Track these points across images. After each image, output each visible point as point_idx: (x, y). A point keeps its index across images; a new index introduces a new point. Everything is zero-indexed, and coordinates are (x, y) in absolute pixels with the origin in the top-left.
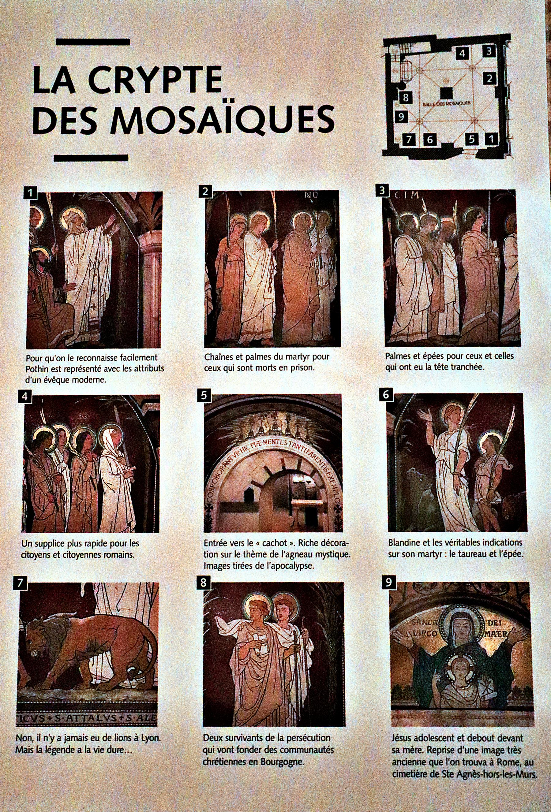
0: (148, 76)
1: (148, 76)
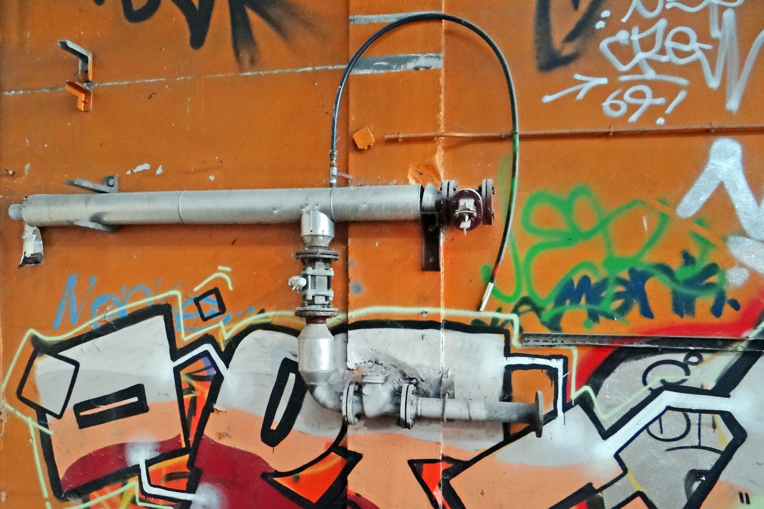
0: (157, 174)
1: (157, 174)
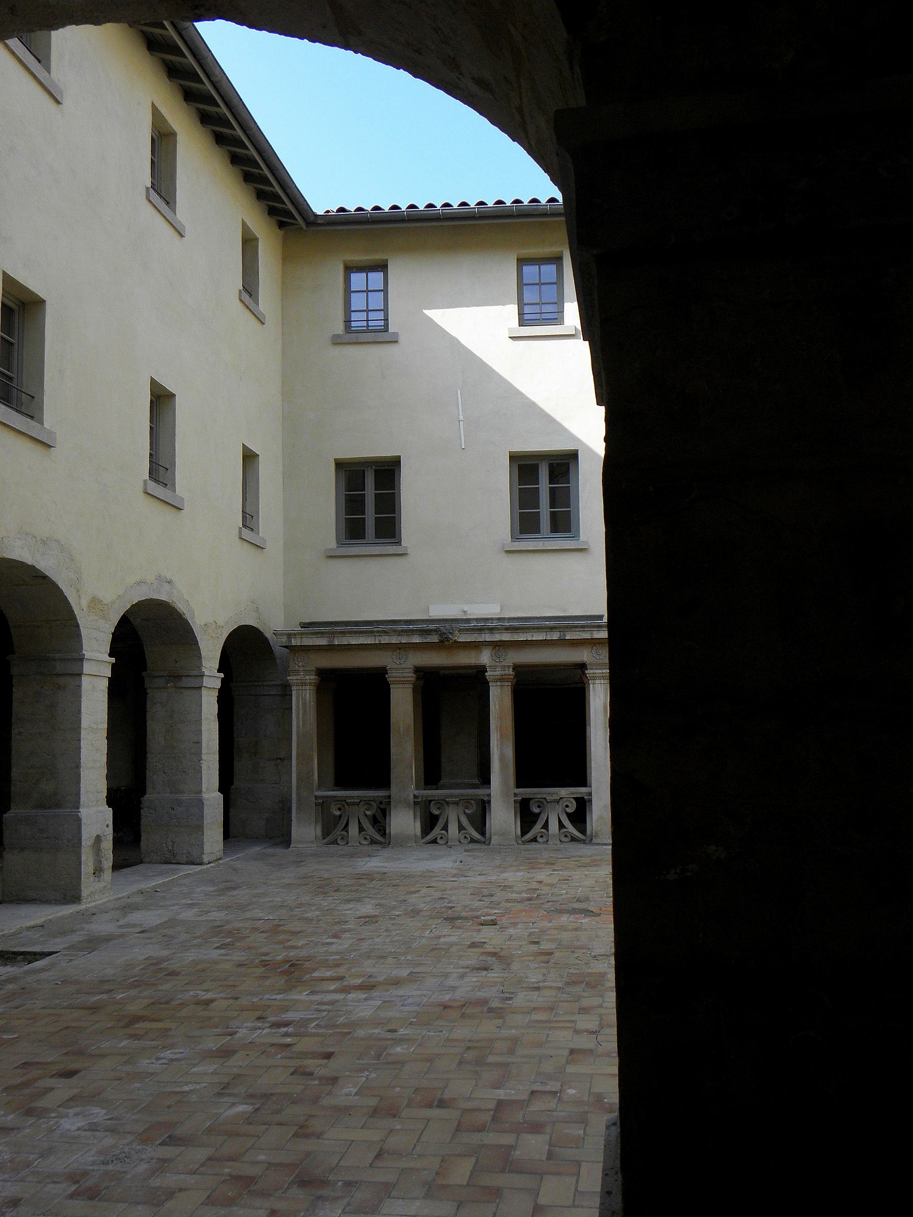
1: (424, 311)
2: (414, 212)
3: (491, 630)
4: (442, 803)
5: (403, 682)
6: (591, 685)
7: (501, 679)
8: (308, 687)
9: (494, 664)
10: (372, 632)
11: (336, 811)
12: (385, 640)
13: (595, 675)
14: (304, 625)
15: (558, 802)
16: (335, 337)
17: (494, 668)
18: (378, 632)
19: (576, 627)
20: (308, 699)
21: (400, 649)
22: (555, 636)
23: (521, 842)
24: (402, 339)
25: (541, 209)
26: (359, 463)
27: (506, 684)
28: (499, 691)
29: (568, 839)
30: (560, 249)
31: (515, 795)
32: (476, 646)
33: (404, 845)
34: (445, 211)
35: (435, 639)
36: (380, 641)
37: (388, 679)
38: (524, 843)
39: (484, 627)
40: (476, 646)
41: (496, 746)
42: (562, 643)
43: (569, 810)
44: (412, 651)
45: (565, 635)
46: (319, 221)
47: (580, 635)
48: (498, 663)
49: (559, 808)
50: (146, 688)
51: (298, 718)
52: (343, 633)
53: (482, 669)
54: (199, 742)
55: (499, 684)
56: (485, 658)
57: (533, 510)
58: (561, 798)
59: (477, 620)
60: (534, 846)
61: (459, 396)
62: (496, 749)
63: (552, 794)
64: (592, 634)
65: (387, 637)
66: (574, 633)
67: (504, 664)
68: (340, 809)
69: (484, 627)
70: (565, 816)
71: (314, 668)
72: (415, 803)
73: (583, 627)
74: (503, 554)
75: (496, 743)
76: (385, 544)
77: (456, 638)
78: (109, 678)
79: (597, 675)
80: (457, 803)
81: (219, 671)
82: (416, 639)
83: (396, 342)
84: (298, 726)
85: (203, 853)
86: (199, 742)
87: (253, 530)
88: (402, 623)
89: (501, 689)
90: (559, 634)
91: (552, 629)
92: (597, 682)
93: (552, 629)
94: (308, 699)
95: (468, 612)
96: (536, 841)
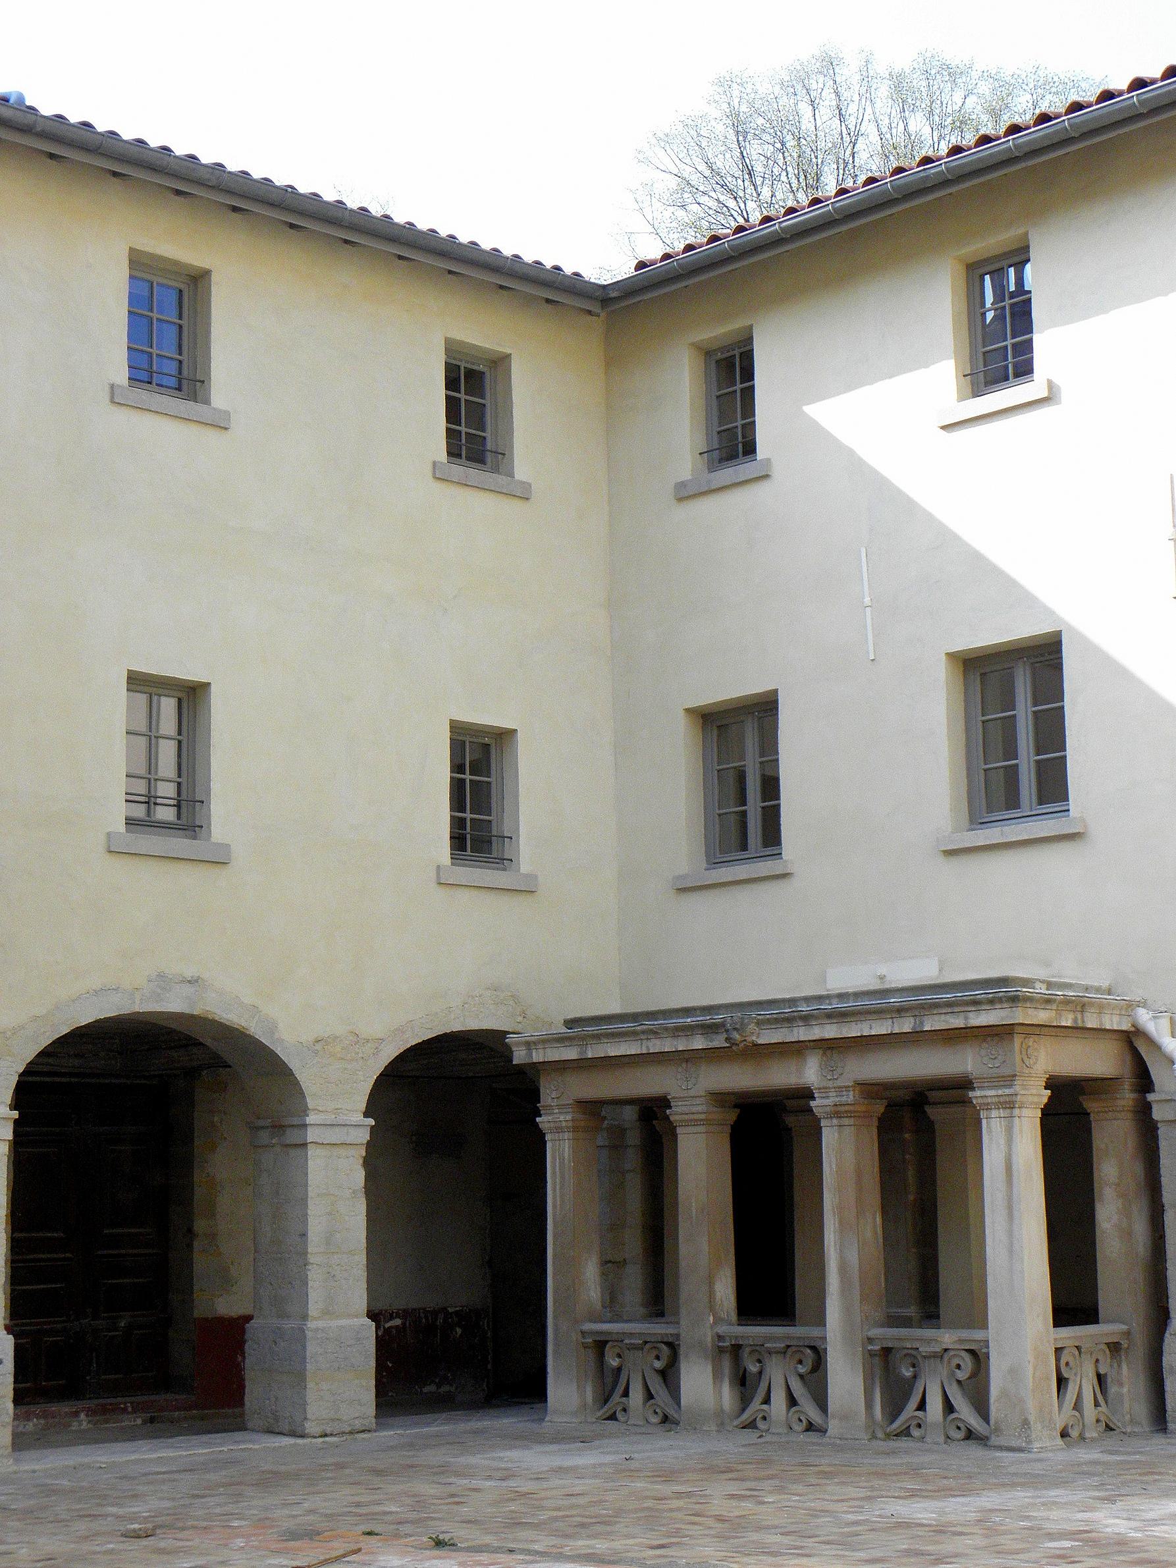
0: (806, 409)
1: (806, 409)
2: (691, 258)
3: (806, 1019)
4: (761, 1353)
5: (696, 1123)
6: (984, 1122)
7: (837, 1113)
8: (566, 1135)
9: (825, 1084)
10: (634, 1033)
11: (907, 1370)
12: (655, 1046)
13: (985, 1101)
14: (570, 1023)
15: (942, 1357)
16: (681, 485)
17: (824, 1089)
18: (643, 1032)
19: (936, 1006)
20: (566, 1155)
21: (687, 1062)
22: (906, 1025)
23: (880, 1435)
24: (777, 471)
25: (933, 174)
26: (739, 708)
27: (846, 1121)
28: (836, 1134)
29: (960, 1435)
30: (1021, 231)
31: (870, 1340)
32: (797, 1050)
33: (698, 1427)
34: (784, 224)
35: (719, 1041)
36: (649, 1049)
37: (672, 1118)
38: (888, 1436)
39: (793, 1014)
40: (797, 1050)
41: (832, 1243)
42: (916, 1038)
43: (962, 1375)
44: (703, 1068)
45: (922, 1023)
46: (614, 294)
47: (947, 1022)
48: (831, 1082)
49: (943, 1370)
50: (544, 1134)
51: (554, 1190)
52: (597, 1037)
53: (806, 1094)
54: (304, 1235)
55: (835, 1121)
56: (811, 1073)
57: (1048, 756)
58: (946, 1350)
59: (842, 996)
60: (903, 1443)
61: (864, 559)
62: (832, 1249)
63: (929, 1341)
64: (966, 1018)
65: (658, 1042)
66: (936, 1018)
67: (839, 1083)
68: (619, 1356)
69: (793, 1014)
70: (955, 1386)
71: (571, 1102)
72: (721, 1350)
73: (949, 1004)
74: (941, 859)
75: (832, 1236)
76: (764, 858)
77: (754, 1038)
78: (9, 1140)
79: (989, 1100)
80: (783, 1352)
81: (366, 1114)
82: (699, 1043)
83: (767, 476)
84: (554, 1206)
85: (306, 1418)
86: (304, 1235)
87: (511, 860)
88: (698, 1012)
89: (839, 1133)
90: (912, 1019)
91: (900, 1011)
92: (994, 1113)
93: (900, 1011)
94: (566, 1155)
95: (888, 978)
96: (908, 1435)
